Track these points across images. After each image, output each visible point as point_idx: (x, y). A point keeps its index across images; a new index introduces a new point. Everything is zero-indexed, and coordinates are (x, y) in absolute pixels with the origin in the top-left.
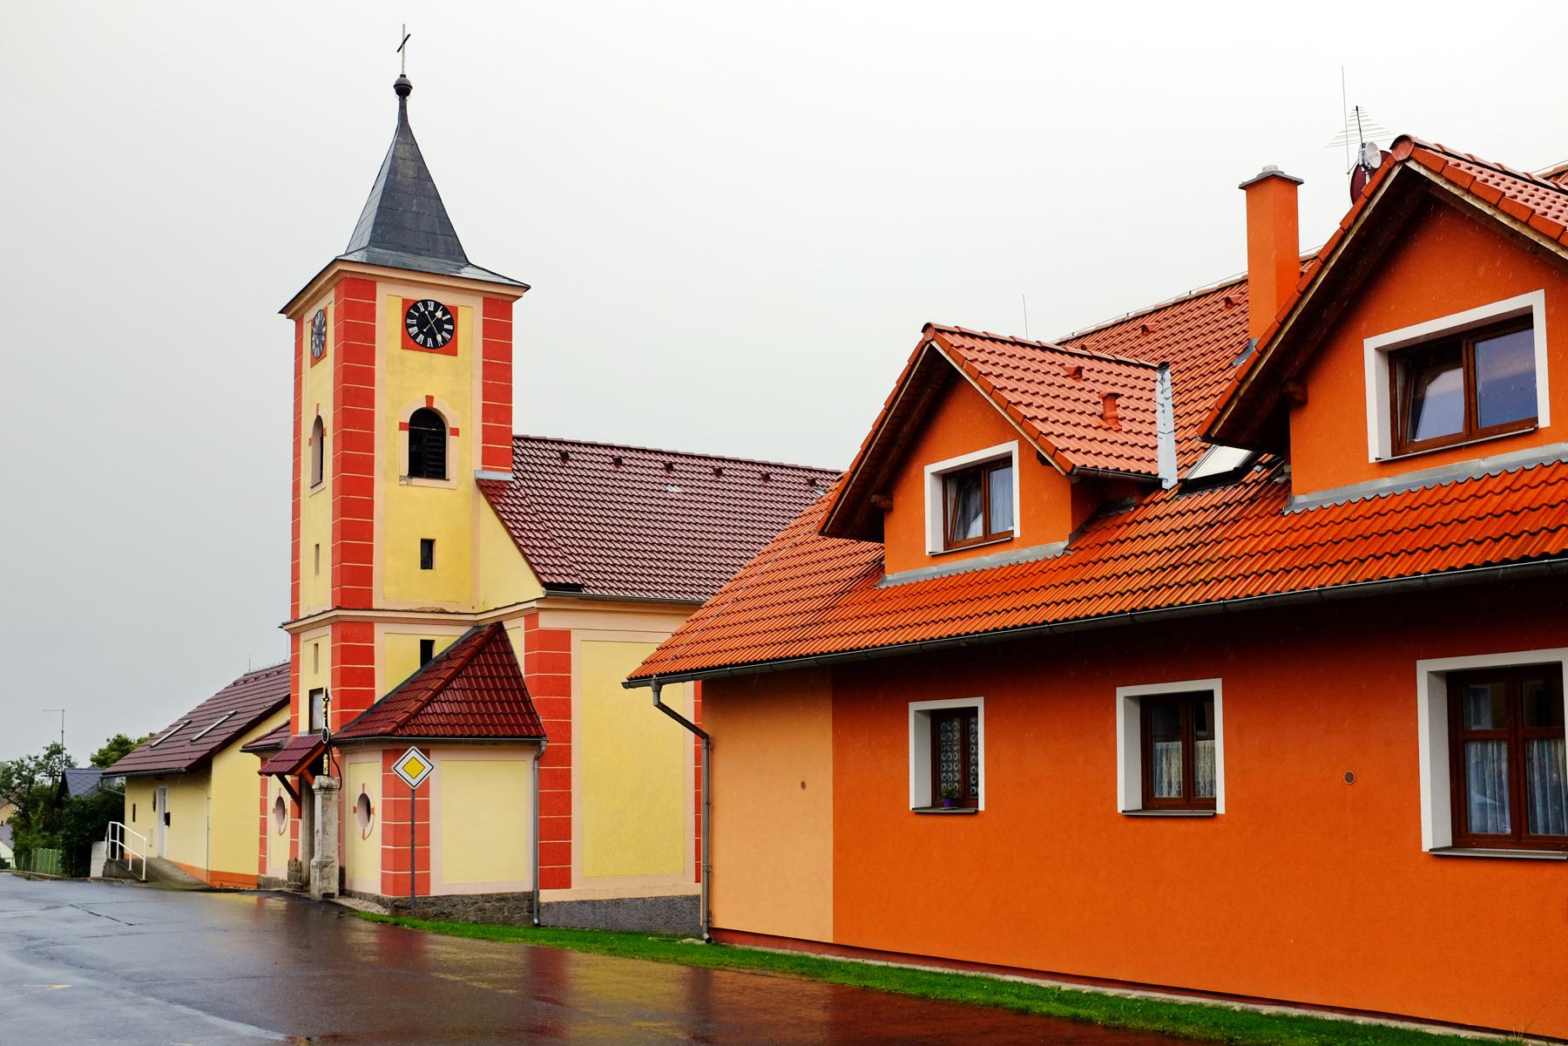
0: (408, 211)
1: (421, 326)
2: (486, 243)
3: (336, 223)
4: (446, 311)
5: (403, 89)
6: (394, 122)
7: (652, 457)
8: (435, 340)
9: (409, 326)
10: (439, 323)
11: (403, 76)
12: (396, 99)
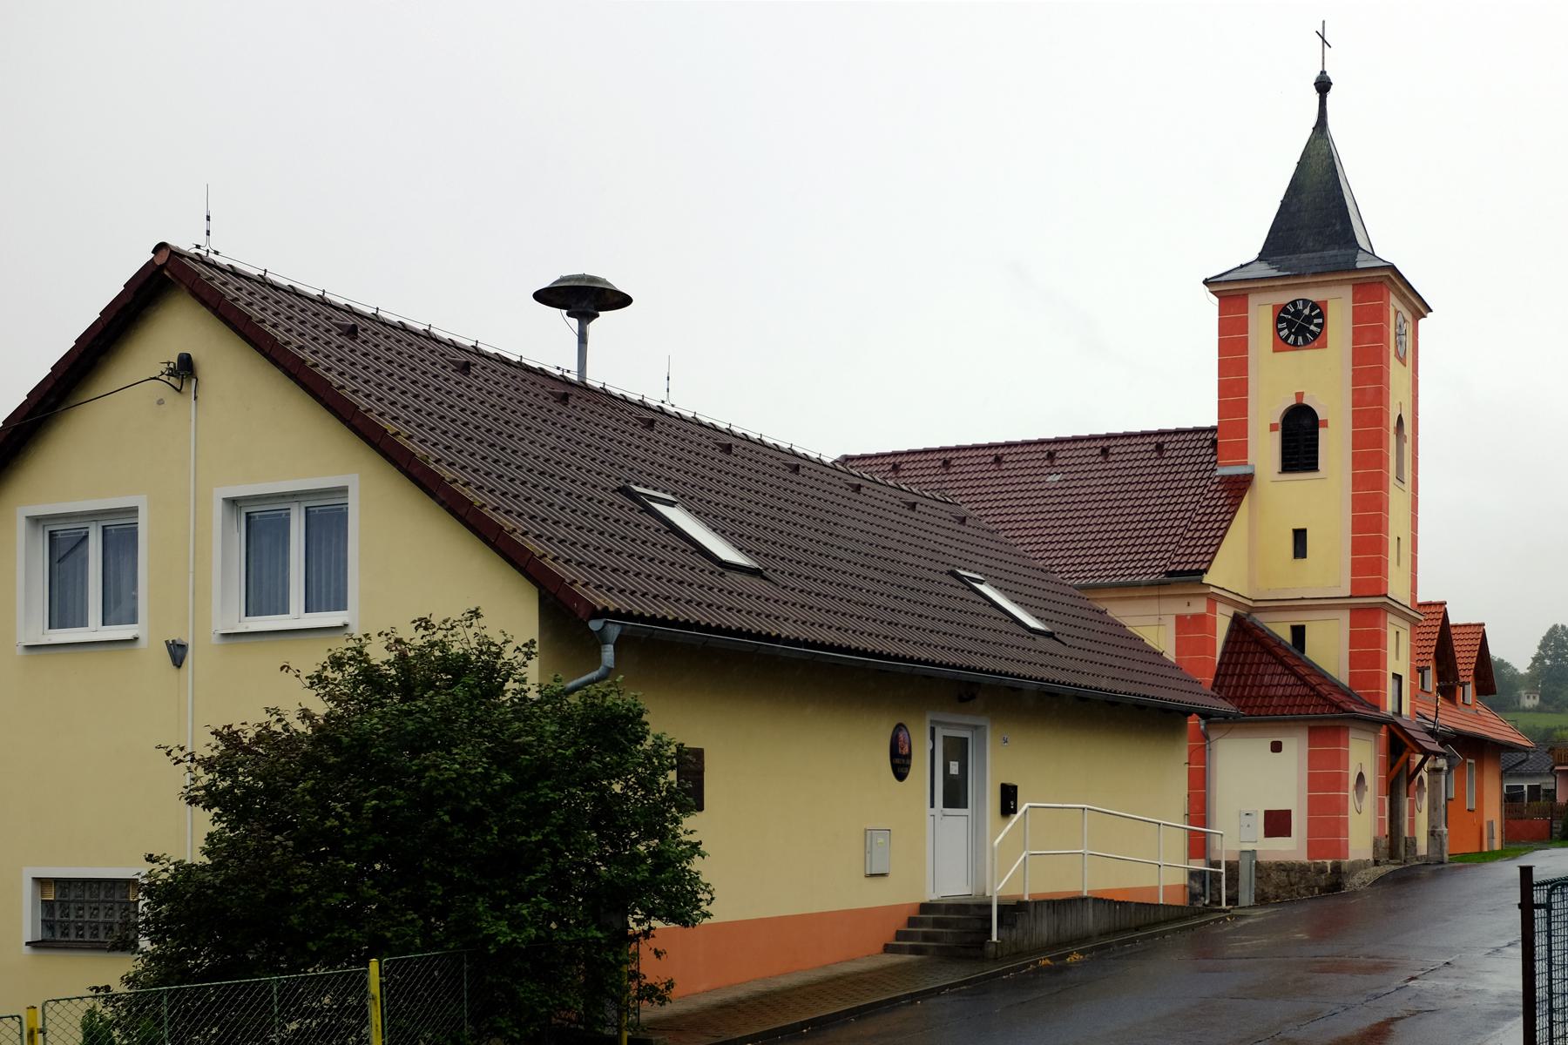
0: (1316, 216)
1: (1290, 325)
2: (1387, 228)
3: (1242, 238)
4: (1314, 306)
5: (1323, 85)
6: (1313, 120)
7: (969, 453)
8: (1312, 333)
9: (1279, 330)
10: (1309, 319)
11: (1323, 72)
12: (1316, 97)
